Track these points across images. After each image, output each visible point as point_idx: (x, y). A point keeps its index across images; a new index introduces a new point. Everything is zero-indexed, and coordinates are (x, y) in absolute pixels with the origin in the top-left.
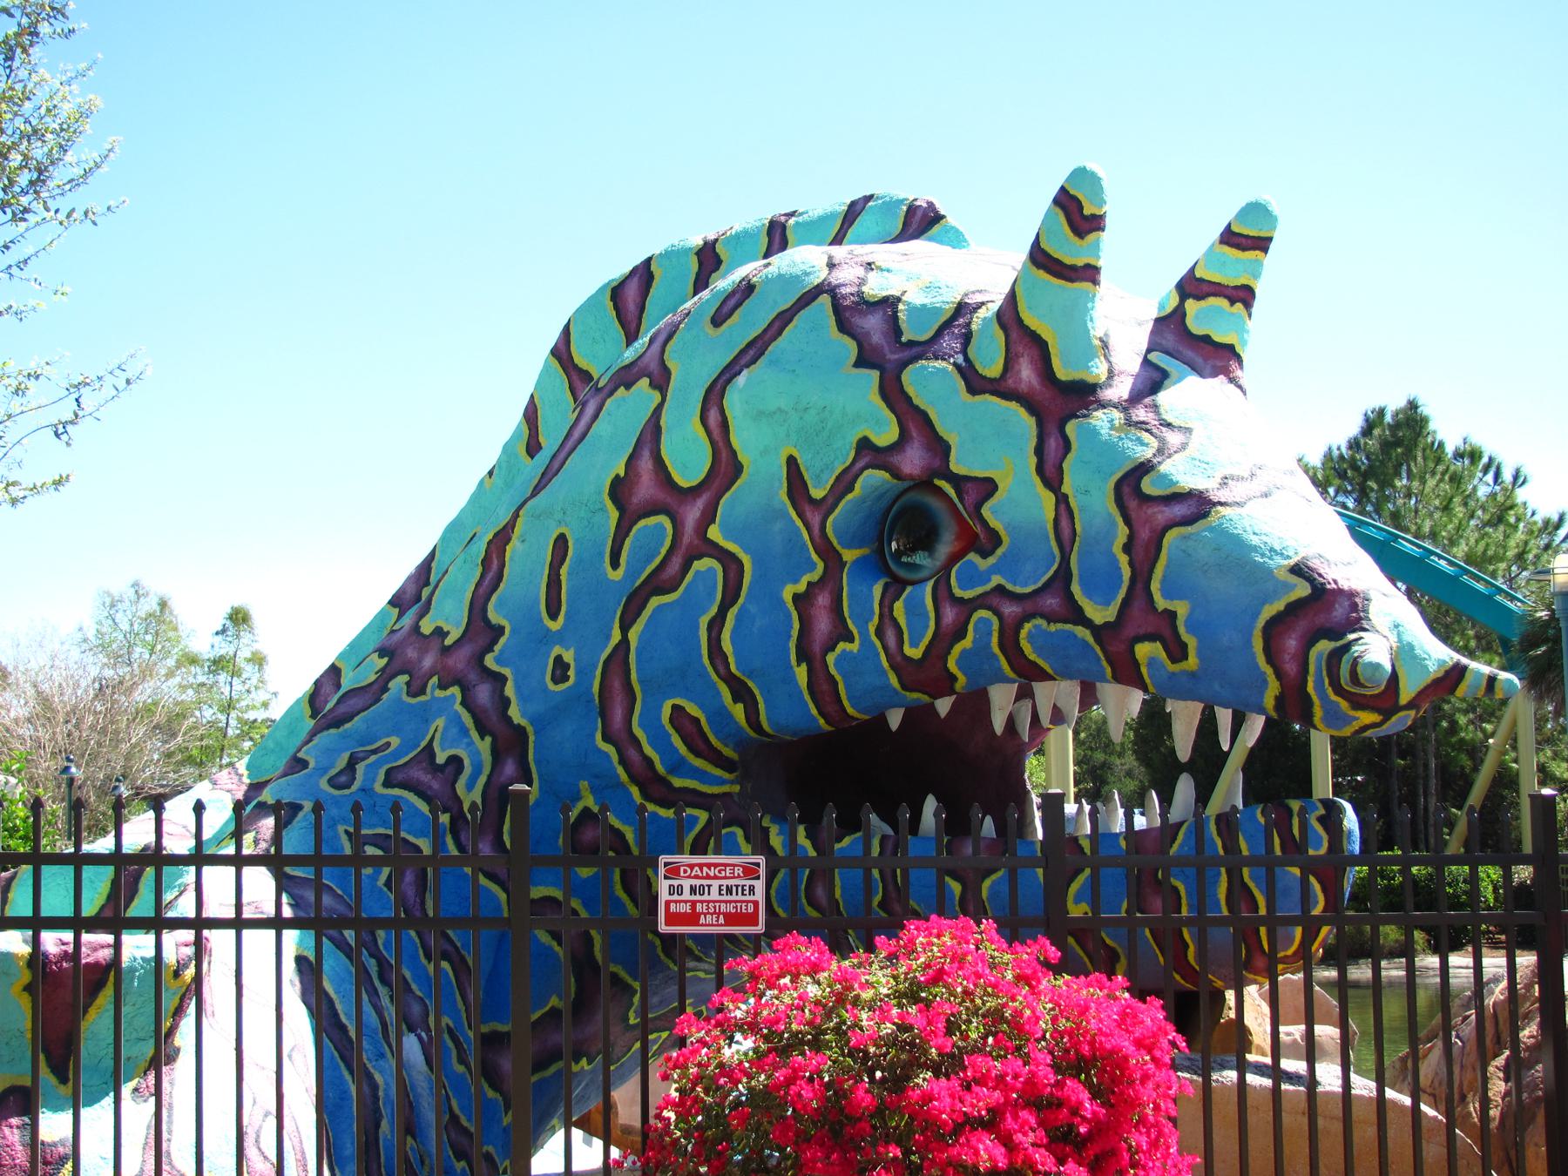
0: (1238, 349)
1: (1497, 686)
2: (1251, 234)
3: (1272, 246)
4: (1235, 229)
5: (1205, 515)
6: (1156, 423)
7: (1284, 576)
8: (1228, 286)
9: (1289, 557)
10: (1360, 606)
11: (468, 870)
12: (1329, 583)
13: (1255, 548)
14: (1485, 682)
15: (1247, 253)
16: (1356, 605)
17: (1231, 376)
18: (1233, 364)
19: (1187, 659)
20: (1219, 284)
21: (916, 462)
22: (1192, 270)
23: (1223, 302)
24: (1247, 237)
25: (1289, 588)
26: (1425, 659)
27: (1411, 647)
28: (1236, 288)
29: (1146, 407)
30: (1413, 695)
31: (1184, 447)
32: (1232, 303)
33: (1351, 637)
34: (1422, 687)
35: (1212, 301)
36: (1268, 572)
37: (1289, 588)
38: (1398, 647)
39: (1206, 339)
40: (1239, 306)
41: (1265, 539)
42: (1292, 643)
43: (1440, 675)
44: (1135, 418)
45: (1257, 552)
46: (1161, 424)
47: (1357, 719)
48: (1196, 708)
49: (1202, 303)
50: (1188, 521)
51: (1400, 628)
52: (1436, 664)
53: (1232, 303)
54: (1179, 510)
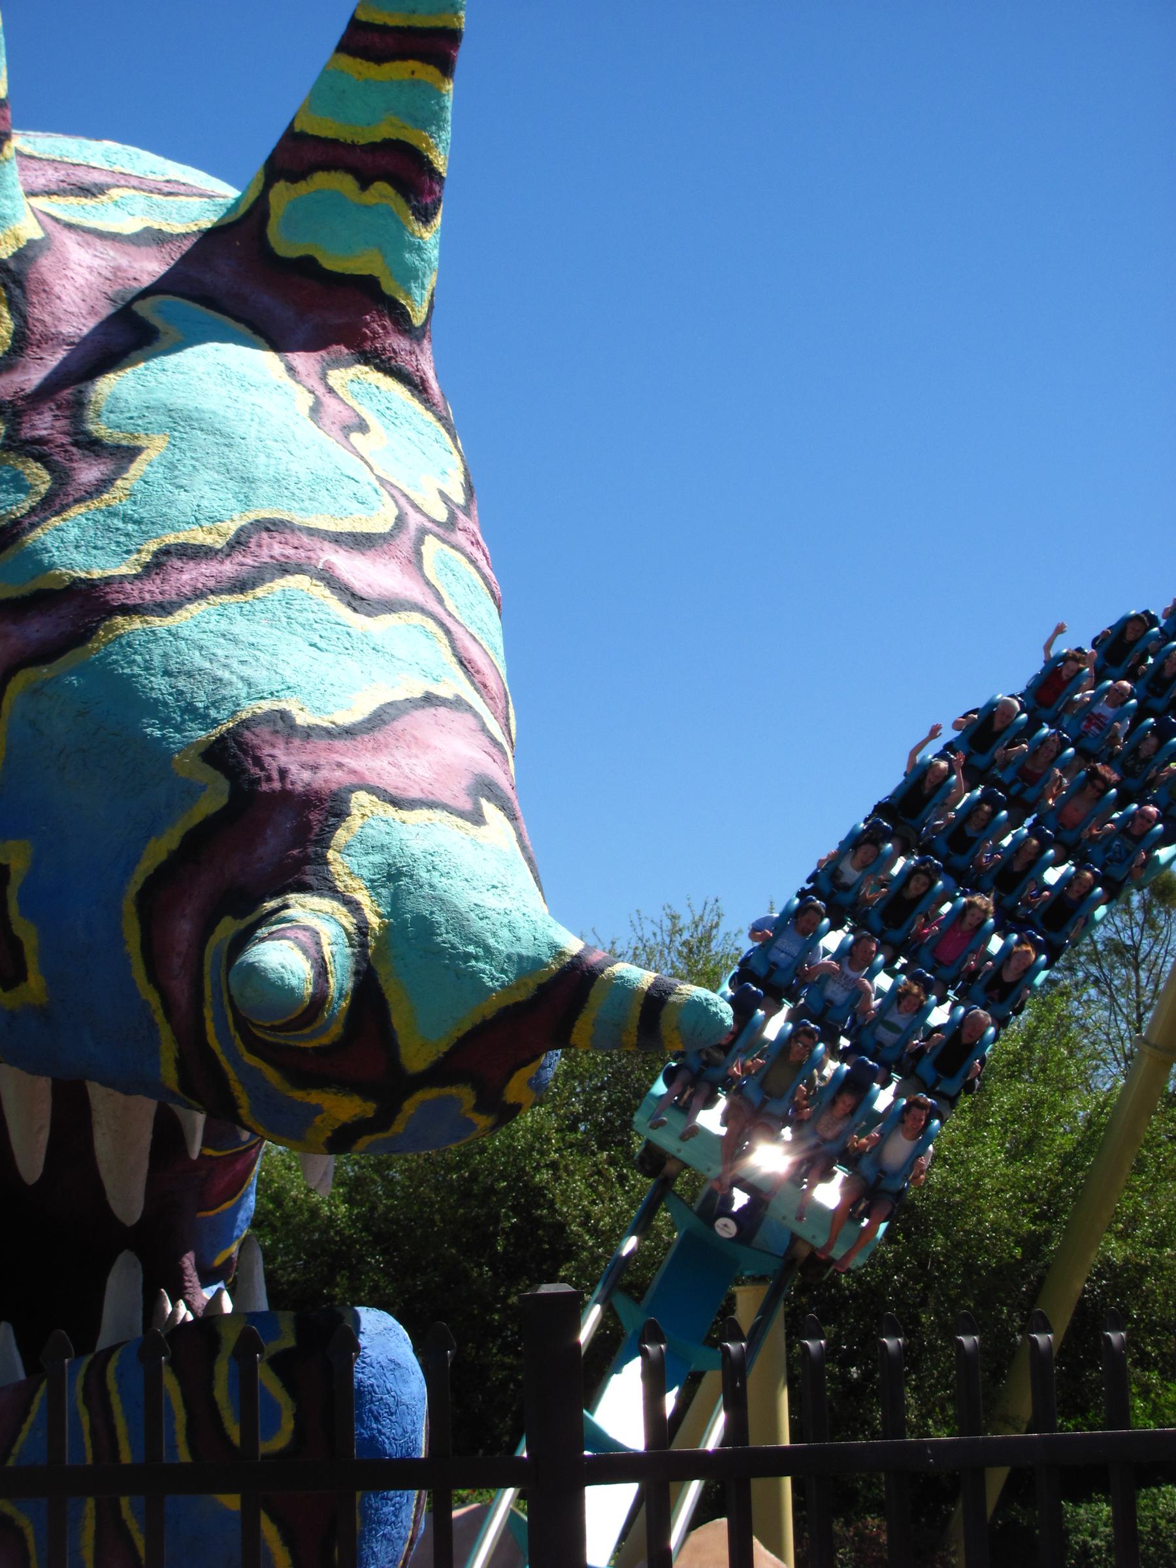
0: (388, 286)
1: (667, 1020)
2: (391, 22)
3: (339, 28)
4: (363, 17)
5: (82, 636)
6: (66, 440)
7: (188, 767)
8: (353, 146)
9: (216, 722)
10: (317, 830)
11: (232, 1502)
12: (269, 779)
13: (153, 707)
14: (636, 1011)
15: (387, 67)
16: (308, 826)
17: (368, 346)
18: (375, 324)
19: (25, 979)
20: (334, 142)
21: (36, 627)
22: (291, 125)
23: (344, 183)
24: (384, 29)
25: (191, 792)
26: (468, 956)
27: (426, 926)
28: (373, 147)
29: (59, 407)
30: (444, 1048)
31: (104, 485)
32: (365, 183)
33: (271, 905)
34: (467, 1027)
35: (322, 180)
36: (158, 751)
37: (191, 792)
38: (386, 928)
39: (307, 266)
40: (382, 189)
41: (181, 683)
42: (184, 928)
43: (521, 996)
44: (27, 433)
45: (154, 714)
46: (76, 444)
47: (318, 1110)
48: (145, 1109)
49: (302, 188)
50: (46, 654)
51: (404, 881)
52: (512, 971)
53: (365, 183)
54: (37, 629)
